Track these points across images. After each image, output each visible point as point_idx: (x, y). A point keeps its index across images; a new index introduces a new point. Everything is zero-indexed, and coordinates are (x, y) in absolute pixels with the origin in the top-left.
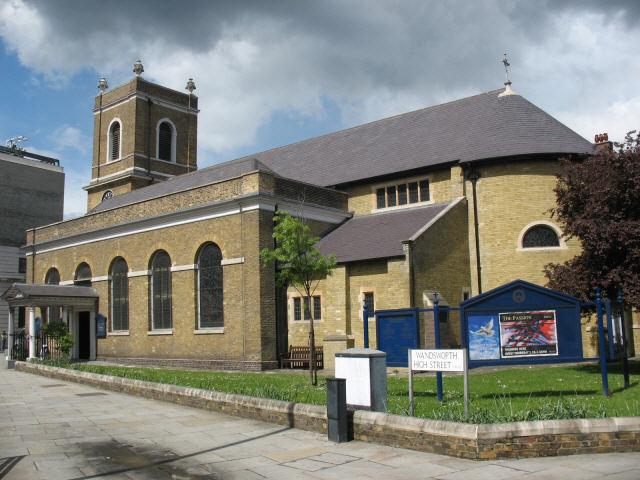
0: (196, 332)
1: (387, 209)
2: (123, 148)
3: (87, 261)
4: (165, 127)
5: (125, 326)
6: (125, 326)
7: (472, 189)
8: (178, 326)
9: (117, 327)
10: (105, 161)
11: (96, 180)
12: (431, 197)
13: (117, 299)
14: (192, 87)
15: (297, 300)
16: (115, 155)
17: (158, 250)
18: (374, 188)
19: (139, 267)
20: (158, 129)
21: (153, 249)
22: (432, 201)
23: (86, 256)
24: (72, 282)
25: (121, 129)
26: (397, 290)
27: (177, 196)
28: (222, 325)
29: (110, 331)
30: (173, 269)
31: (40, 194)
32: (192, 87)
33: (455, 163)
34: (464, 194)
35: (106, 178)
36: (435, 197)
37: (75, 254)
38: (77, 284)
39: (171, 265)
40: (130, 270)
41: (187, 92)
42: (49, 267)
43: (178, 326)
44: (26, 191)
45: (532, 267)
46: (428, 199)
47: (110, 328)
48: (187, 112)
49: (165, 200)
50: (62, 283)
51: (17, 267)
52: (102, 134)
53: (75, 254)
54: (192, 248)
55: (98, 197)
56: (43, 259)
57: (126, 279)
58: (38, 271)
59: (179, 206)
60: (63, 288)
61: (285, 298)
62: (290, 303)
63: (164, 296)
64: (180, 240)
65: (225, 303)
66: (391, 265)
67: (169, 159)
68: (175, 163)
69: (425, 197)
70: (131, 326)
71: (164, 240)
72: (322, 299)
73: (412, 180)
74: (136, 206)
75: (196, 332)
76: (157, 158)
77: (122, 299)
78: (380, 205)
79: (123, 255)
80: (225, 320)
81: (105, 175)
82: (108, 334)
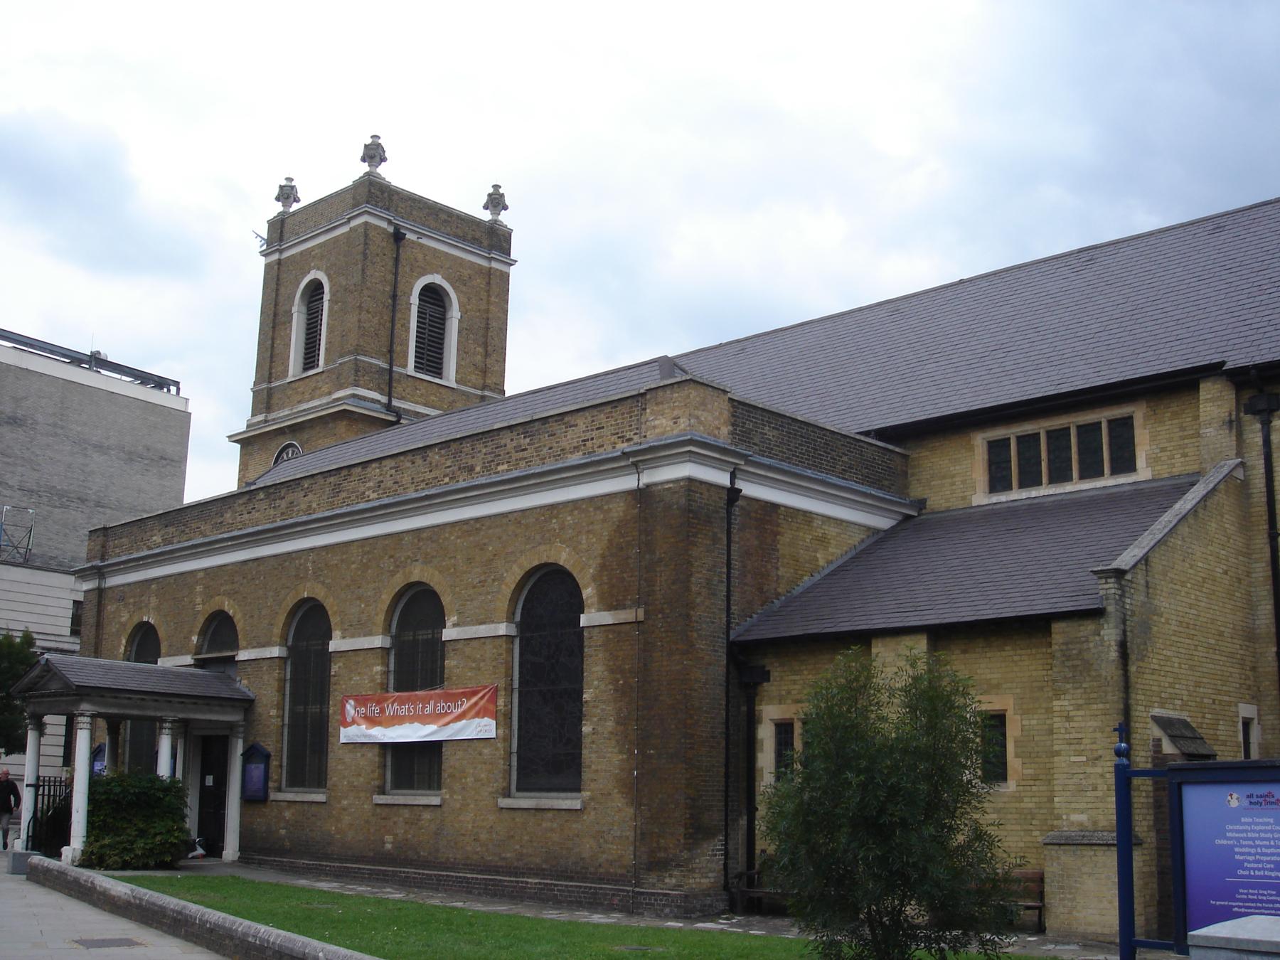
0: (504, 802)
1: (1017, 495)
2: (329, 343)
3: (229, 607)
4: (433, 295)
5: (318, 779)
6: (318, 779)
7: (1259, 440)
8: (457, 786)
9: (297, 779)
10: (285, 373)
11: (261, 418)
12: (1141, 462)
13: (300, 708)
14: (496, 201)
15: (784, 730)
16: (310, 359)
17: (410, 586)
18: (980, 441)
19: (363, 628)
20: (415, 300)
21: (398, 582)
22: (1143, 472)
23: (229, 594)
24: (188, 660)
25: (326, 297)
26: (1079, 708)
27: (467, 447)
28: (578, 789)
29: (279, 790)
30: (449, 634)
31: (131, 457)
32: (496, 201)
33: (1213, 370)
34: (1239, 454)
35: (284, 416)
36: (1152, 461)
37: (199, 588)
38: (200, 664)
39: (443, 625)
40: (337, 634)
41: (486, 216)
42: (136, 620)
43: (457, 786)
44: (99, 448)
45: (80, 719)
46: (1130, 467)
47: (439, 343)
48: (484, 263)
49: (434, 456)
50: (165, 663)
51: (69, 622)
52: (281, 309)
53: (199, 588)
54: (500, 579)
55: (263, 459)
56: (122, 599)
57: (326, 658)
58: (111, 629)
59: (471, 469)
60: (166, 673)
61: (752, 721)
62: (766, 734)
63: (314, 709)
64: (470, 560)
65: (586, 729)
66: (1057, 627)
67: (438, 371)
68: (454, 385)
69: (1125, 463)
70: (333, 779)
71: (428, 560)
72: (1013, 731)
73: (1028, 428)
74: (359, 470)
75: (504, 802)
76: (410, 369)
77: (314, 709)
78: (998, 482)
79: (320, 593)
80: (586, 775)
81: (282, 407)
82: (273, 796)
